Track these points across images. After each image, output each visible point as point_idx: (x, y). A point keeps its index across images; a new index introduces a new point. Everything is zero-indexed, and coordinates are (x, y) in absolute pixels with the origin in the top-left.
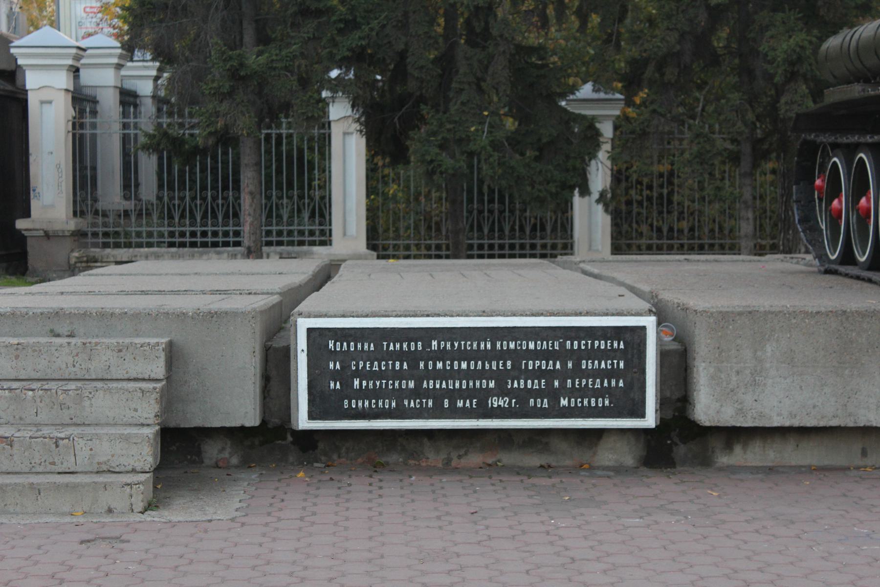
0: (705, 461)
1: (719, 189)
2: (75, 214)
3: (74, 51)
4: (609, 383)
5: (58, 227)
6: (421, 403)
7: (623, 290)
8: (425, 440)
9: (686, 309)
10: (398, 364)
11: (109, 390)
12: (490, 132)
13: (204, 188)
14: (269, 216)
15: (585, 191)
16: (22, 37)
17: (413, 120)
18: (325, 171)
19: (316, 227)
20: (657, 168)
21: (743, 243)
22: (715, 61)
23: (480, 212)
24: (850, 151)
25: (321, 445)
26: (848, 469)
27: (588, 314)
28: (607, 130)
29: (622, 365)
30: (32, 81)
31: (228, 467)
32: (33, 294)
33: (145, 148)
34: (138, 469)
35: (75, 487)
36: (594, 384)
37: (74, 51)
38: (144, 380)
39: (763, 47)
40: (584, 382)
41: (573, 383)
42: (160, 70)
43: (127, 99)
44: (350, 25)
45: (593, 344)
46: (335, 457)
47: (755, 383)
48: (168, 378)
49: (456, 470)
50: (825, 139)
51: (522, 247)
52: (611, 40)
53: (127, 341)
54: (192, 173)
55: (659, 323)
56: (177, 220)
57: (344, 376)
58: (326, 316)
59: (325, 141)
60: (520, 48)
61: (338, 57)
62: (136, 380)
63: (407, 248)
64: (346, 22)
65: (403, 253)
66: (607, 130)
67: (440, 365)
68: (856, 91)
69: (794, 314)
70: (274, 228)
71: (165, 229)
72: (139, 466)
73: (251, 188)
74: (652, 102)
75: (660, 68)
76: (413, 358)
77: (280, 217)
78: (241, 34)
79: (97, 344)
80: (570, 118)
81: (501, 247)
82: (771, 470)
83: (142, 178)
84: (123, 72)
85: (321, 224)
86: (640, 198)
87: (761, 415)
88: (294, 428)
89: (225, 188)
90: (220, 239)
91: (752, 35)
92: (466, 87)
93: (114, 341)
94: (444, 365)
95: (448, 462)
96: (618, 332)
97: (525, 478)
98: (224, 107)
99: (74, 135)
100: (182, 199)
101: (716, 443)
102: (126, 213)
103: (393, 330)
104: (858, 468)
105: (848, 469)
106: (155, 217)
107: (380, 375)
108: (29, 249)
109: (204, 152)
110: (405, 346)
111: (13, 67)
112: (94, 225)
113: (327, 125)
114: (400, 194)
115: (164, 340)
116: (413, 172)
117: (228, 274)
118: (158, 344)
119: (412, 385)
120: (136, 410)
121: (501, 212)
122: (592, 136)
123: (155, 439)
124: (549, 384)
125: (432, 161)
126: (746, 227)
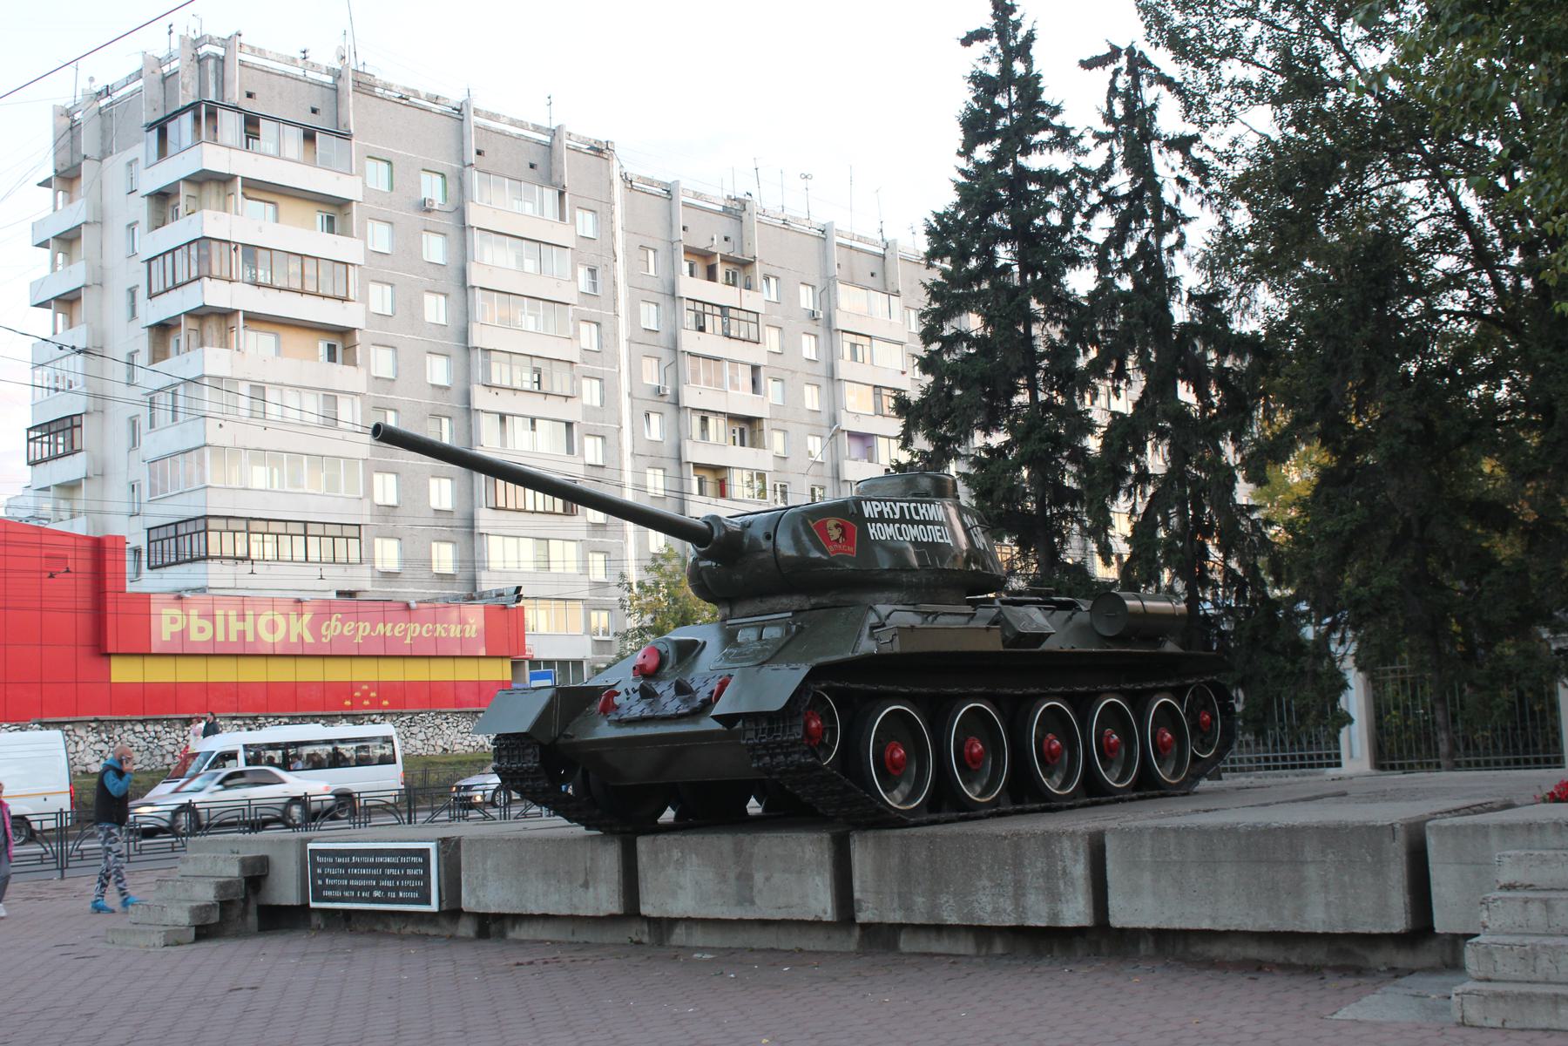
0: (502, 935)
25: (353, 919)
47: (483, 885)
126: (1444, 748)
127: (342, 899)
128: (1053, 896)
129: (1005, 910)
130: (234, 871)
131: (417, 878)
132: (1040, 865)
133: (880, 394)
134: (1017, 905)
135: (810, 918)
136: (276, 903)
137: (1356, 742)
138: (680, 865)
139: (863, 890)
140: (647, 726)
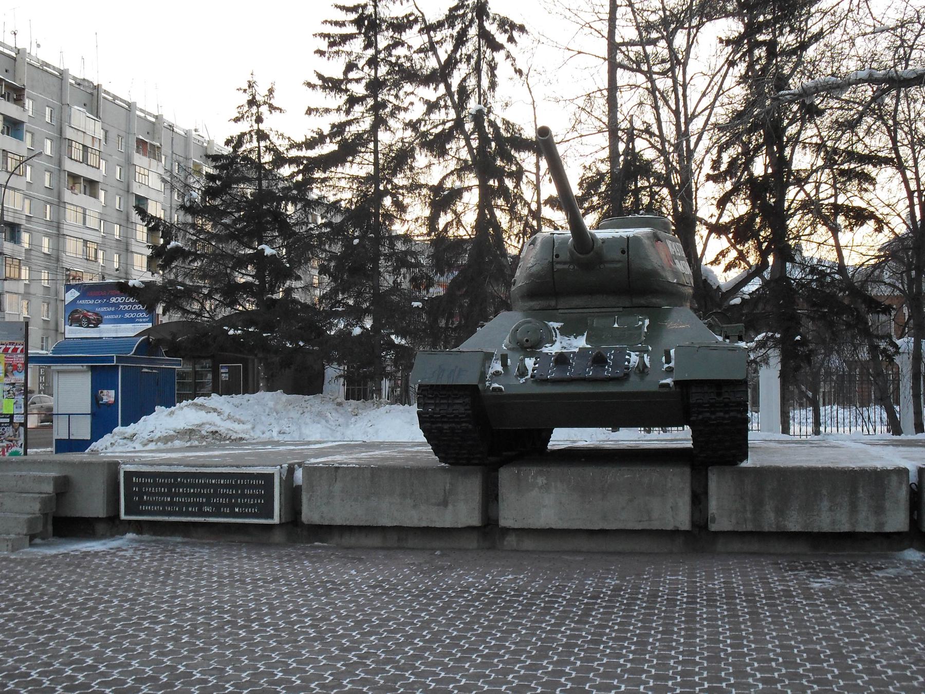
57: (140, 494)
128: (879, 510)
130: (49, 488)
131: (260, 496)
133: (7, 157)
135: (670, 528)
136: (69, 515)
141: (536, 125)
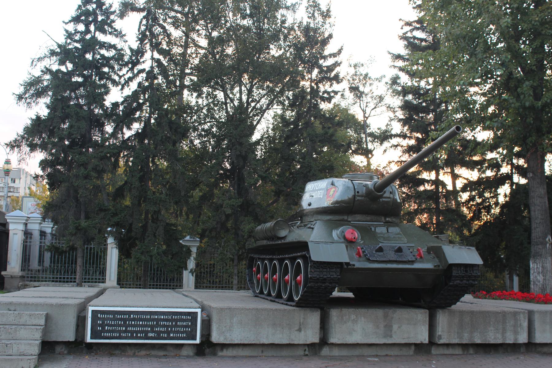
0: (214, 354)
1: (227, 270)
2: (22, 270)
3: (26, 218)
4: (186, 329)
5: (15, 274)
6: (127, 335)
7: (192, 301)
8: (128, 347)
9: (210, 307)
10: (120, 322)
11: (26, 328)
12: (157, 249)
13: (65, 263)
14: (86, 273)
15: (186, 269)
16: (9, 213)
17: (133, 245)
18: (105, 259)
19: (101, 277)
20: (209, 263)
21: (234, 287)
22: (227, 230)
23: (154, 274)
24: (263, 260)
25: (94, 348)
26: (258, 357)
27: (180, 308)
28: (194, 250)
29: (190, 324)
30: (11, 227)
31: (63, 354)
32: (4, 297)
33: (47, 250)
34: (33, 354)
35: (12, 360)
36: (181, 329)
37: (26, 218)
38: (37, 325)
39: (242, 227)
40: (178, 329)
41: (175, 329)
42: (54, 225)
43: (43, 234)
44: (115, 215)
45: (181, 317)
46: (98, 351)
48: (46, 325)
49: (137, 356)
50: (256, 256)
51: (167, 285)
52: (196, 222)
53: (33, 313)
54: (62, 258)
55: (202, 311)
56: (55, 273)
57: (102, 325)
58: (98, 306)
59: (106, 249)
60: (167, 224)
61: (110, 224)
62: (35, 325)
63: (130, 285)
64: (114, 214)
65: (128, 286)
66: (194, 250)
67: (133, 323)
68: (265, 242)
69: (242, 309)
70: (87, 277)
71: (51, 276)
72: (33, 353)
73: (80, 264)
74: (208, 242)
75: (210, 232)
76: (125, 320)
77: (89, 273)
78: (80, 216)
79: (23, 313)
80: (182, 246)
81: (160, 285)
82: (234, 357)
83: (45, 259)
84: (42, 225)
85: (102, 276)
86: (204, 271)
87: (232, 340)
88: (86, 342)
89: (72, 263)
90: (87, 280)
91: (238, 223)
92: (150, 235)
93: (29, 313)
94: (135, 323)
95: (134, 354)
96: (189, 314)
97: (158, 359)
98: (73, 238)
99: (24, 245)
100: (58, 266)
101: (218, 348)
102: (39, 271)
103: (119, 311)
104: (260, 356)
105: (258, 357)
106: (48, 272)
107: (114, 325)
108: (5, 281)
109: (66, 252)
110: (123, 316)
111: (5, 222)
112: (28, 274)
113: (106, 245)
114: (129, 268)
115: (45, 313)
116: (132, 260)
117: (69, 292)
118: (43, 314)
119: (124, 329)
120: (34, 335)
121: (161, 274)
122: (189, 252)
123: (39, 345)
124: (167, 329)
125: (138, 258)
126: (235, 282)
127: (120, 338)
128: (516, 333)
129: (498, 338)
132: (512, 322)
134: (503, 336)
137: (188, 279)
138: (355, 321)
139: (443, 331)
140: (406, 264)
141: (114, 288)
